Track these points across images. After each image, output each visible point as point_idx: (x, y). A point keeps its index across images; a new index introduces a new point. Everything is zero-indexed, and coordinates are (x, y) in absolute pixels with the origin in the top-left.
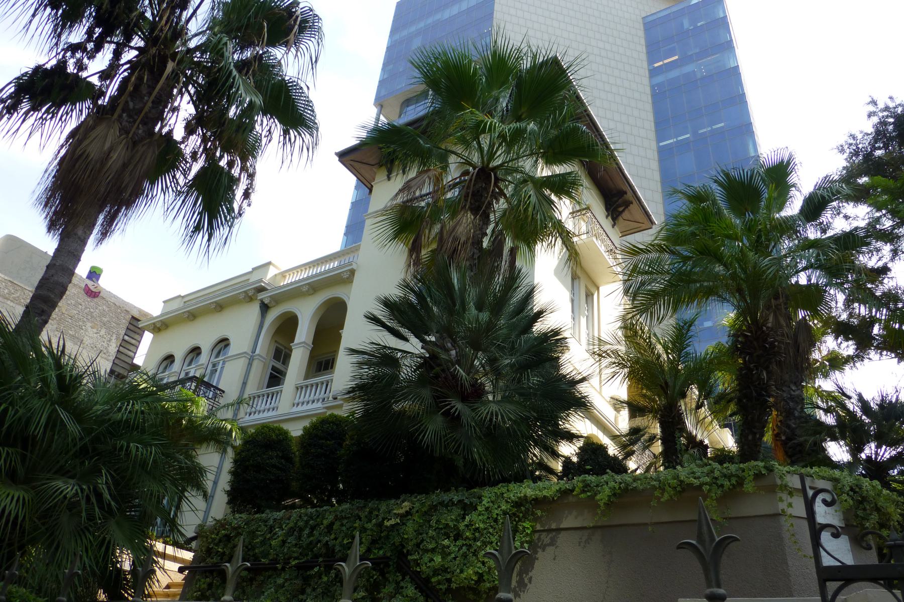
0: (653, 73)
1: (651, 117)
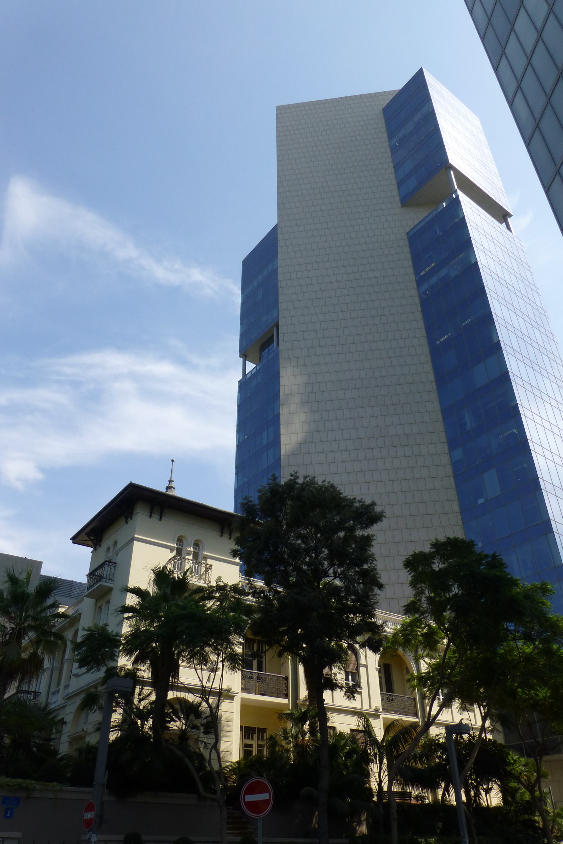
0: (420, 282)
1: (421, 324)
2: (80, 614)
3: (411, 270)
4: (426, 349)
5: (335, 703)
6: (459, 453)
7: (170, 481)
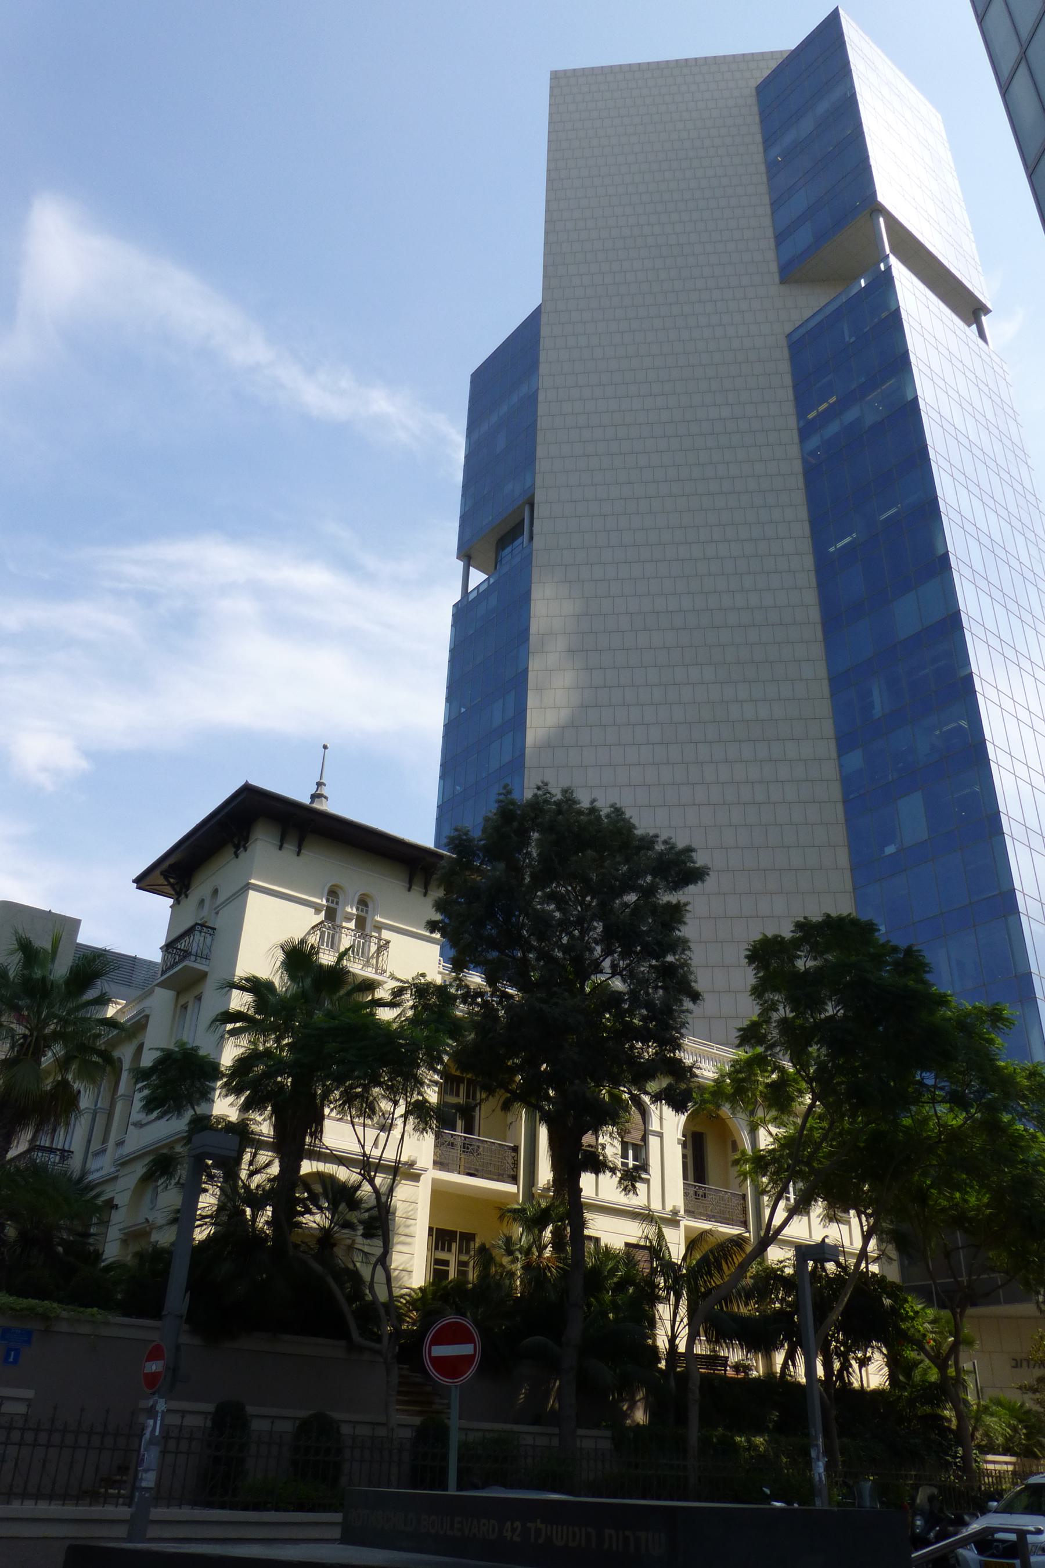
0: (805, 433)
1: (803, 513)
2: (147, 1017)
3: (789, 408)
4: (809, 562)
5: (600, 1196)
6: (856, 759)
7: (319, 784)
